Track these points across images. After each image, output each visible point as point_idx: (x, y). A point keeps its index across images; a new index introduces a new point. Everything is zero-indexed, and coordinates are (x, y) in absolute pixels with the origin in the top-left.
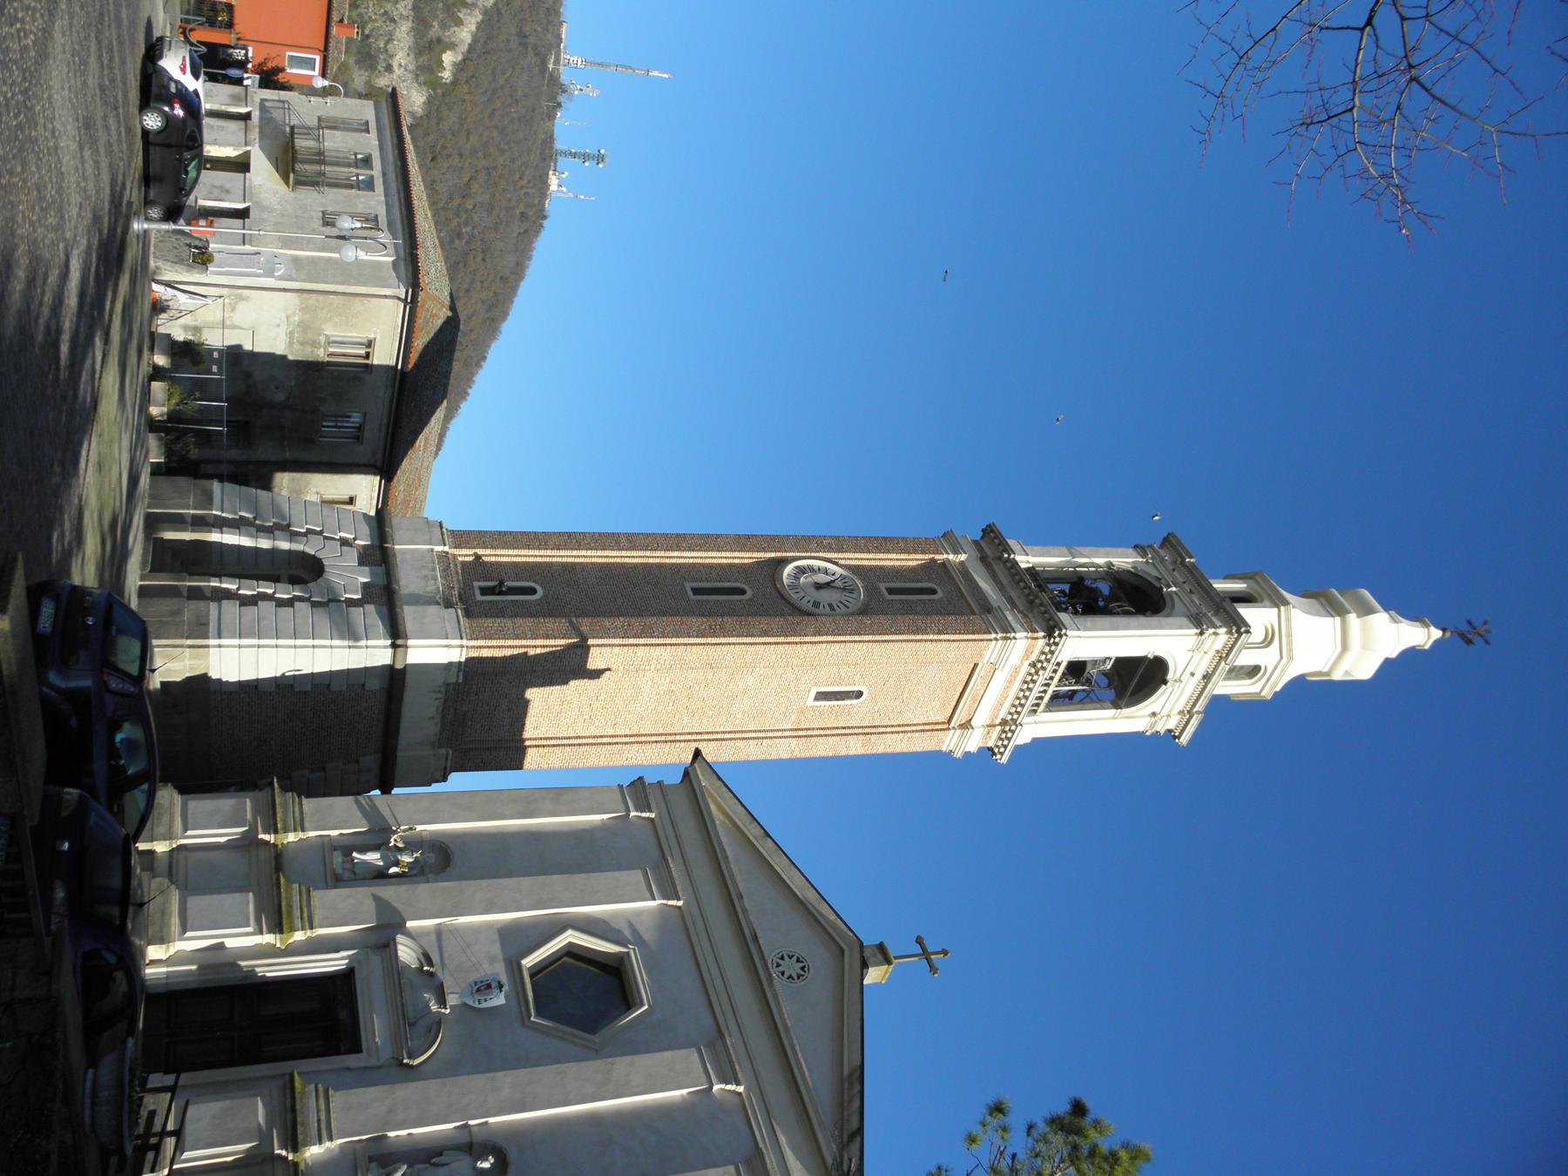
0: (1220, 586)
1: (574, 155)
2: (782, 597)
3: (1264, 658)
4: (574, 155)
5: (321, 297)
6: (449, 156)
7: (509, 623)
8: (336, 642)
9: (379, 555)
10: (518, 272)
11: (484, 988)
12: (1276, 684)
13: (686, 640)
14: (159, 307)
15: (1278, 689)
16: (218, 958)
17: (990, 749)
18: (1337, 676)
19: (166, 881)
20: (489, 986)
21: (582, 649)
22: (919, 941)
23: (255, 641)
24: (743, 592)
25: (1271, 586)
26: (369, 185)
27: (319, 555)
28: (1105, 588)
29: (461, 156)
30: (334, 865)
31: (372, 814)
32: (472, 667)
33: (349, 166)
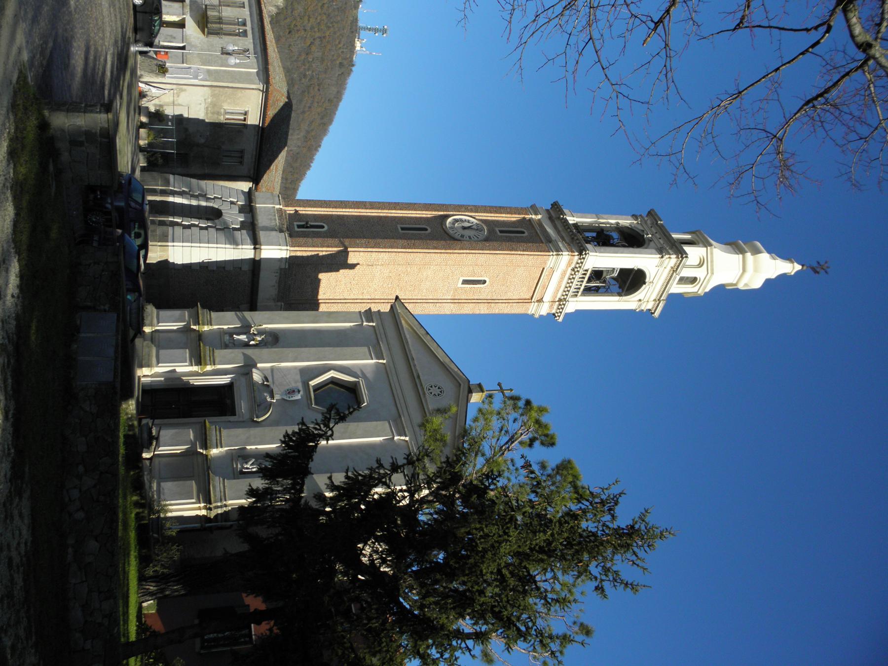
0: (675, 236)
1: (370, 30)
2: (445, 232)
3: (700, 273)
4: (370, 30)
5: (221, 89)
6: (298, 31)
7: (310, 240)
8: (227, 246)
9: (248, 209)
10: (338, 96)
11: (292, 392)
12: (705, 287)
13: (396, 250)
14: (142, 95)
15: (707, 290)
16: (173, 375)
17: (554, 314)
18: (741, 286)
19: (150, 343)
20: (294, 391)
21: (345, 253)
22: (499, 384)
23: (190, 244)
24: (426, 230)
25: (704, 237)
26: (245, 33)
27: (220, 208)
28: (615, 235)
29: (305, 30)
30: (226, 341)
31: (243, 320)
32: (292, 261)
33: (235, 24)
